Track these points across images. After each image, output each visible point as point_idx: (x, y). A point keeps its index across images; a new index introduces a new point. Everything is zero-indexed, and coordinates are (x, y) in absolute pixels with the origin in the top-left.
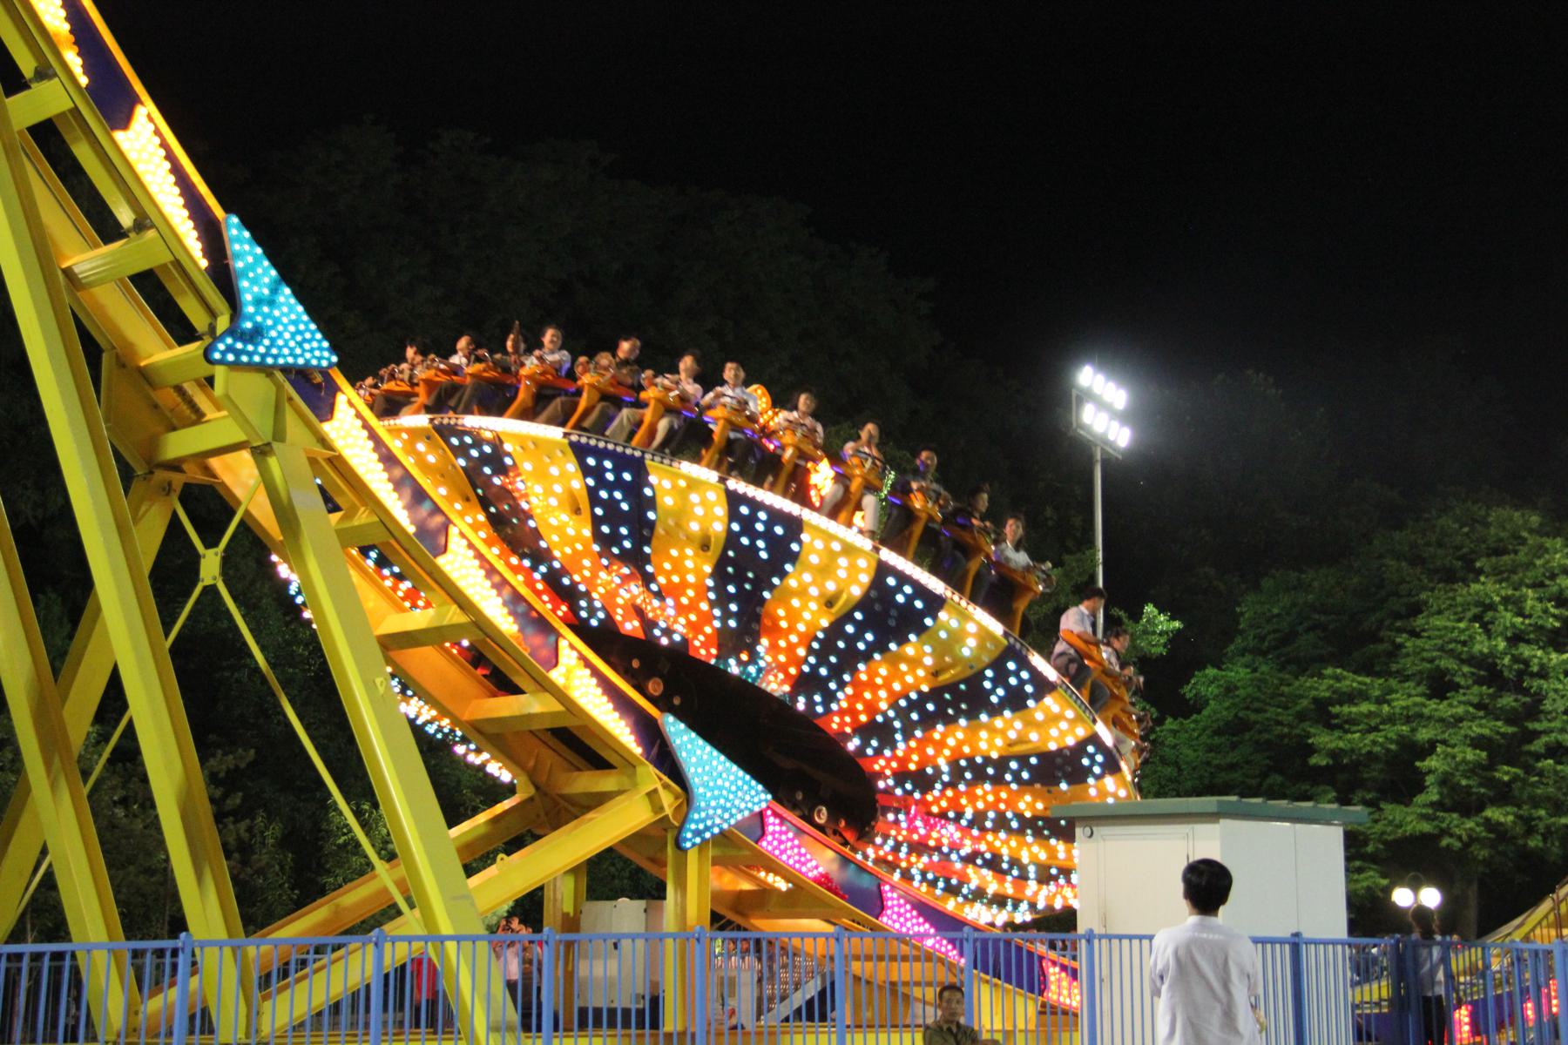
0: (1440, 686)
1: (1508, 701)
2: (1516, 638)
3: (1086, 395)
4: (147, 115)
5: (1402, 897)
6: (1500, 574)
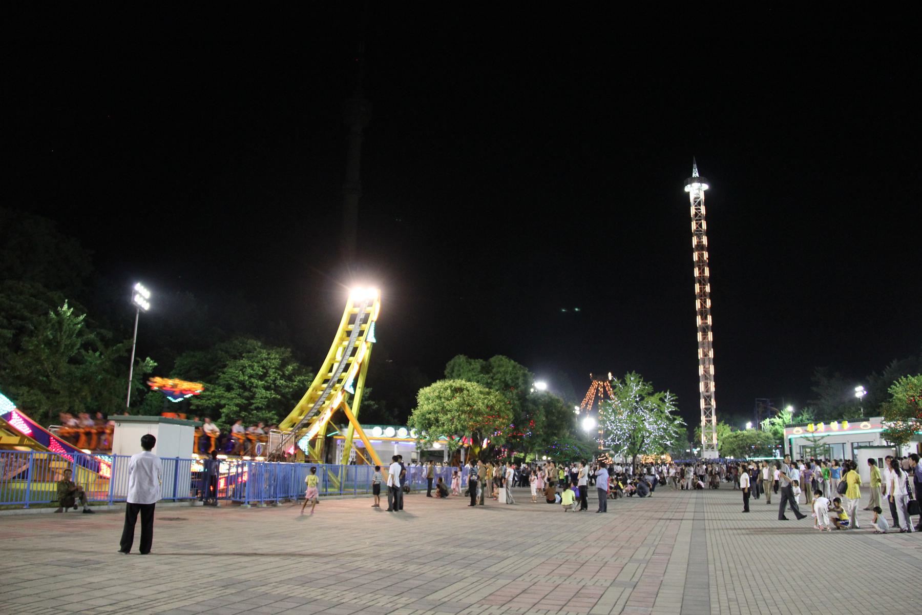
0: (229, 388)
1: (247, 394)
2: (251, 376)
6: (249, 358)
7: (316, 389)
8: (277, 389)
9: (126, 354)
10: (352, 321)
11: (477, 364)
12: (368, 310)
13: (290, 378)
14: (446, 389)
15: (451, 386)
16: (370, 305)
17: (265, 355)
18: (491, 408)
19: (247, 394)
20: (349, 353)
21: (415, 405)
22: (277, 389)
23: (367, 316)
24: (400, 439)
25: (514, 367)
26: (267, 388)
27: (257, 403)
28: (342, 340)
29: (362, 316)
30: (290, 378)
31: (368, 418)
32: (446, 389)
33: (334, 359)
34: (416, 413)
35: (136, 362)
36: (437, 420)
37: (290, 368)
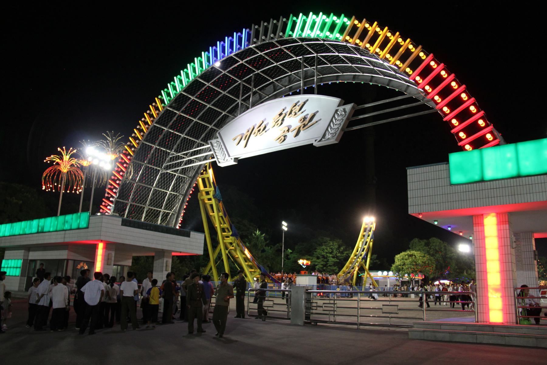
0: (318, 258)
1: (325, 260)
2: (327, 253)
3: (287, 227)
4: (211, 169)
5: (301, 262)
6: (325, 245)
7: (352, 259)
8: (337, 257)
9: (280, 248)
10: (365, 231)
11: (423, 243)
12: (371, 226)
13: (342, 253)
14: (405, 255)
15: (408, 254)
16: (372, 224)
17: (331, 244)
18: (425, 263)
19: (325, 260)
20: (364, 244)
21: (393, 262)
22: (337, 257)
23: (371, 228)
24: (386, 277)
25: (440, 243)
26: (333, 257)
27: (330, 263)
28: (361, 239)
29: (369, 229)
30: (342, 253)
31: (374, 267)
32: (405, 255)
33: (358, 246)
34: (394, 266)
35: (284, 251)
36: (403, 268)
37: (342, 248)
